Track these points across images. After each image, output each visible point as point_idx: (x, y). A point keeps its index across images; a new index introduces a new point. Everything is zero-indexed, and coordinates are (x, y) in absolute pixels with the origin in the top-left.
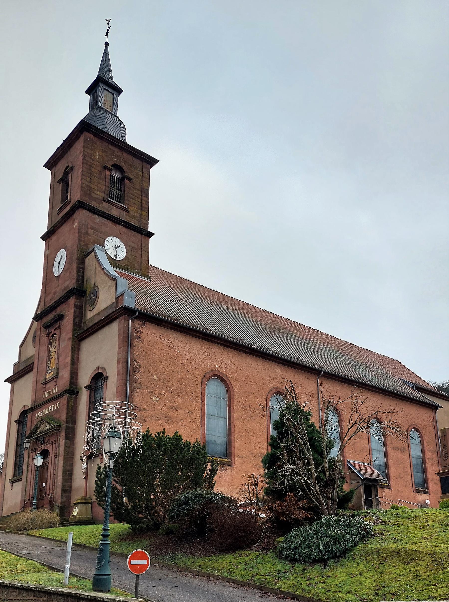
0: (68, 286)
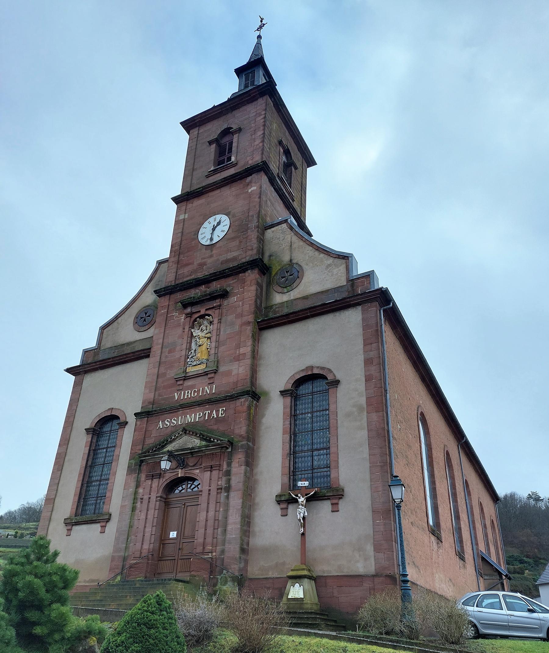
0: (234, 259)
